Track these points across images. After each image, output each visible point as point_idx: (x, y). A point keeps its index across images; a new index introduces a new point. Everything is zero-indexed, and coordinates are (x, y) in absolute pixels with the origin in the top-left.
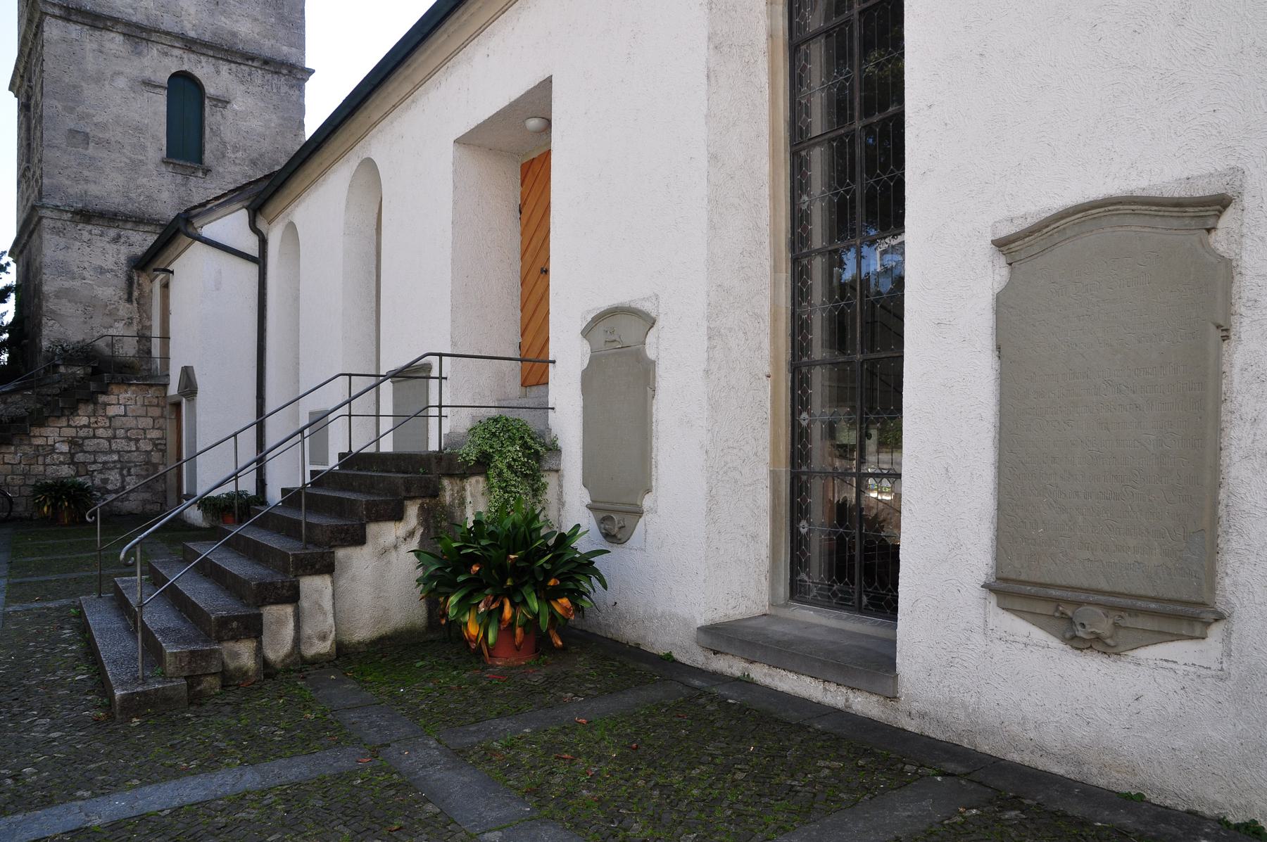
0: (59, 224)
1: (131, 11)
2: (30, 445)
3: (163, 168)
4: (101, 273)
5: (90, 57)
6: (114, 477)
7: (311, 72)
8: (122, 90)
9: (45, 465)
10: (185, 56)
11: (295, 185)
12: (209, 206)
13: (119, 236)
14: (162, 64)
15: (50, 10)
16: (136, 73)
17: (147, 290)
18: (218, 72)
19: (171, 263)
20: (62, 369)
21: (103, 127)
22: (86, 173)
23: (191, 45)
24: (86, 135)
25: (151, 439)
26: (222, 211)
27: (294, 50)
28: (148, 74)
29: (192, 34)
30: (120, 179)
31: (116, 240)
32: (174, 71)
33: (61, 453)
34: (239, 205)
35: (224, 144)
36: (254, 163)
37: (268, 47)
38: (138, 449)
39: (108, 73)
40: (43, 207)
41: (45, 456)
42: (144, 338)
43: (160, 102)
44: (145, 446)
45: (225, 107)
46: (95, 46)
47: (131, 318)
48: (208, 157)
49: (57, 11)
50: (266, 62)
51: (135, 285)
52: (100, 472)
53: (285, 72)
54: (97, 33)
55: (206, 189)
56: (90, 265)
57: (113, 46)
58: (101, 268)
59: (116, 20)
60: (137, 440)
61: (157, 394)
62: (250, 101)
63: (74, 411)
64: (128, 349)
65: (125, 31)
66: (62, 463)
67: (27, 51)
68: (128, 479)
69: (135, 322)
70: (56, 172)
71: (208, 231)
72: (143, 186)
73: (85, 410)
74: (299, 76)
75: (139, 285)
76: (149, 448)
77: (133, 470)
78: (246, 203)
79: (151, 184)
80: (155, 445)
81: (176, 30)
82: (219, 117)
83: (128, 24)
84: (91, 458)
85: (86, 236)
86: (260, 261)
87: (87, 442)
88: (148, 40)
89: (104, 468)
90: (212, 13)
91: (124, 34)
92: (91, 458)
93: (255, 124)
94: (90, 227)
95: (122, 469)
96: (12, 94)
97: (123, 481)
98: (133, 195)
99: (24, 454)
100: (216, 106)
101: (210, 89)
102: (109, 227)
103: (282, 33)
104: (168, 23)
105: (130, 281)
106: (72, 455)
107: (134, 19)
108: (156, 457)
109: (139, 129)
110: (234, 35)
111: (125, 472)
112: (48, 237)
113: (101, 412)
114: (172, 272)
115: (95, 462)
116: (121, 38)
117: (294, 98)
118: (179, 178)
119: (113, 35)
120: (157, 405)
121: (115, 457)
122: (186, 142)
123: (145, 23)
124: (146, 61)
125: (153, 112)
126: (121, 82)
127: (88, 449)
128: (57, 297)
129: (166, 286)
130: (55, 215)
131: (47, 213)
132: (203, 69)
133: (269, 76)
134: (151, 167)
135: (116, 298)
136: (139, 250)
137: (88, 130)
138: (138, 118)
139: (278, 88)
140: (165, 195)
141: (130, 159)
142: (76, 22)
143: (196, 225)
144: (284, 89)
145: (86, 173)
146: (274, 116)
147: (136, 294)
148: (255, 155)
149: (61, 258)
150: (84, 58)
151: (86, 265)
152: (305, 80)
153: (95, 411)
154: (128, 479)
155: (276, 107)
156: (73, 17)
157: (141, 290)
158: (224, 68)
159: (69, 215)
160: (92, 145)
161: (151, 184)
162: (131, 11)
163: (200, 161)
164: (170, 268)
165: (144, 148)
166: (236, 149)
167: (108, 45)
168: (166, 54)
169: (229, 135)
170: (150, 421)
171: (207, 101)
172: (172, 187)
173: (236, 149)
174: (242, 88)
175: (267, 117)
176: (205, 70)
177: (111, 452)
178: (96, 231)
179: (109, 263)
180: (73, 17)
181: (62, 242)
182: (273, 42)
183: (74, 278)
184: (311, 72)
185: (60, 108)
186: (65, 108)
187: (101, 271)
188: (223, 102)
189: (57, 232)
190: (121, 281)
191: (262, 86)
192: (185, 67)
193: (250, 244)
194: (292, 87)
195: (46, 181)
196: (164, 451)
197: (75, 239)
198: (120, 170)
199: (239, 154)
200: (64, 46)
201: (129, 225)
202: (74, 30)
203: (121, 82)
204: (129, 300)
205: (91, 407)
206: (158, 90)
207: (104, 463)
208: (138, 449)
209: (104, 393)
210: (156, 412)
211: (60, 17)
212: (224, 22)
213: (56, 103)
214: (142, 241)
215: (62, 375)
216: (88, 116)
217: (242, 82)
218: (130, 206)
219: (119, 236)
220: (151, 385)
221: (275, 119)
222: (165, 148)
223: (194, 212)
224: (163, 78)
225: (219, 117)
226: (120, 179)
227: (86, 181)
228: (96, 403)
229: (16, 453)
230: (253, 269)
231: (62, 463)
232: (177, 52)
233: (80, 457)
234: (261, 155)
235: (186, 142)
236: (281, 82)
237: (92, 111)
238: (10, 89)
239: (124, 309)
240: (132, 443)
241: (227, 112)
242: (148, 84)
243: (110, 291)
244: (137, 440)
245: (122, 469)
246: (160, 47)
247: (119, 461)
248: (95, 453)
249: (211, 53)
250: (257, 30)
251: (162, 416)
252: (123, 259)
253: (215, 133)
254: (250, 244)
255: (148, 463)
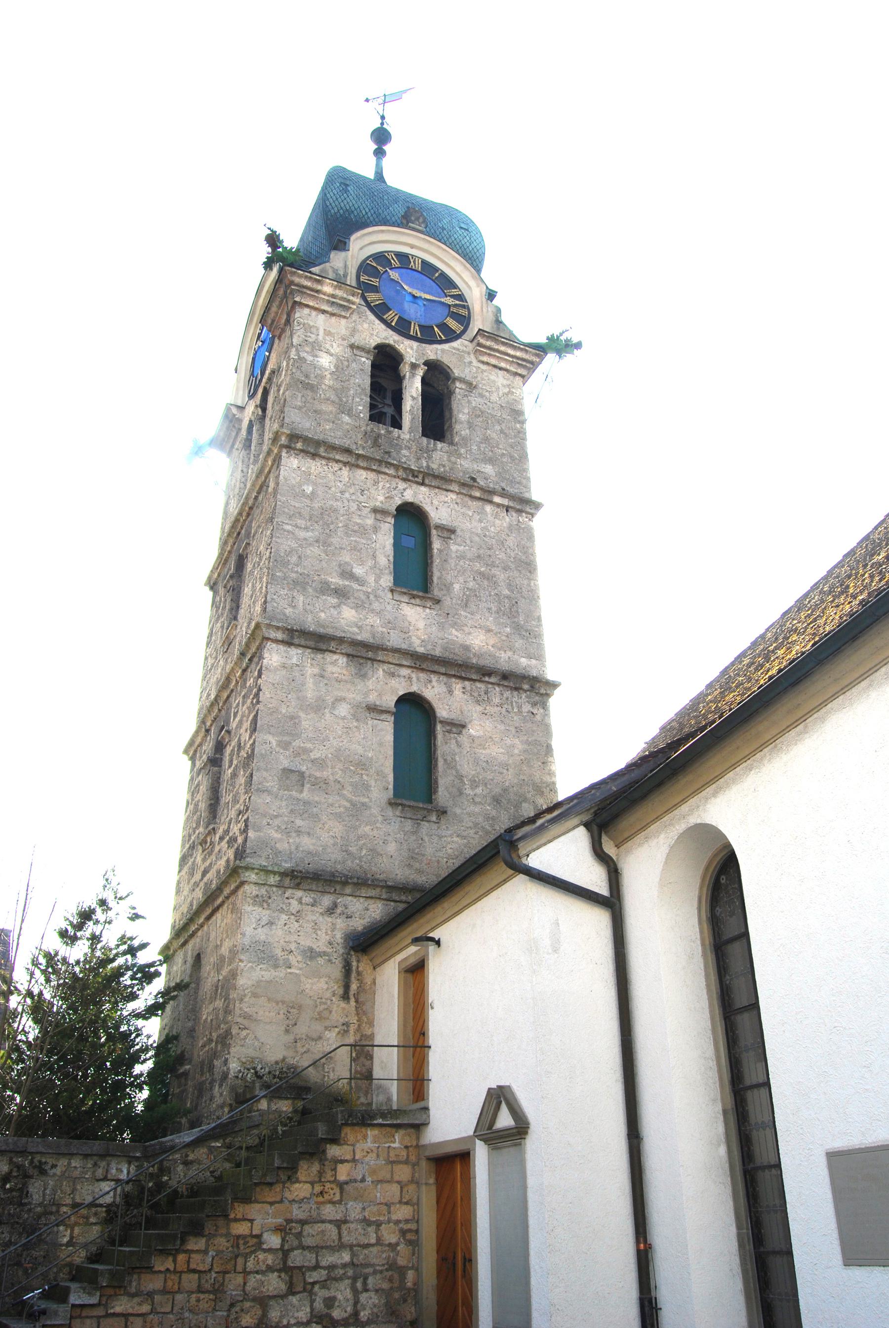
0: (263, 891)
1: (355, 630)
2: (228, 1235)
3: (390, 812)
4: (311, 958)
5: (310, 683)
6: (342, 1292)
7: (554, 685)
8: (344, 718)
9: (246, 1273)
10: (414, 675)
11: (714, 761)
12: (540, 822)
13: (335, 905)
14: (387, 686)
15: (273, 634)
16: (359, 698)
17: (368, 980)
18: (450, 692)
19: (433, 929)
20: (264, 1105)
21: (320, 763)
22: (299, 822)
23: (422, 662)
24: (302, 774)
25: (398, 1222)
26: (555, 829)
27: (534, 662)
28: (372, 698)
29: (421, 650)
30: (338, 829)
31: (331, 911)
32: (401, 693)
33: (270, 1250)
34: (575, 821)
35: (460, 777)
36: (497, 800)
37: (504, 659)
38: (379, 1242)
39: (329, 699)
40: (247, 868)
41: (246, 1256)
42: (363, 1050)
43: (386, 730)
44: (390, 1236)
45: (460, 733)
46: (316, 670)
47: (346, 1024)
48: (442, 795)
49: (280, 635)
50: (505, 676)
51: (354, 975)
52: (324, 1284)
53: (526, 687)
54: (319, 656)
55: (440, 837)
56: (282, 952)
57: (335, 669)
58: (311, 950)
59: (341, 640)
60: (378, 1224)
61: (407, 1141)
62: (488, 724)
63: (290, 1172)
64: (340, 1070)
65: (350, 650)
66: (270, 1269)
67: (225, 695)
68: (363, 1297)
69: (352, 1028)
70: (264, 822)
71: (541, 858)
72: (365, 836)
73: (307, 1170)
74: (542, 691)
75: (359, 973)
76: (393, 1240)
77: (371, 1281)
78: (586, 817)
79: (375, 833)
80: (403, 1232)
81: (404, 646)
82: (453, 745)
83: (355, 643)
84: (309, 1259)
85: (295, 905)
86: (612, 903)
87: (308, 1229)
88: (373, 660)
89: (330, 1278)
90: (442, 626)
91: (348, 655)
92: (309, 1259)
93: (495, 751)
94: (299, 893)
95: (354, 1279)
96: (186, 758)
97: (356, 1302)
98: (353, 849)
99: (219, 1252)
100: (449, 732)
101: (442, 712)
102: (323, 892)
103: (519, 643)
104: (394, 640)
105: (347, 969)
106: (285, 1253)
107: (359, 638)
108: (403, 1256)
109: (362, 765)
110: (467, 648)
111: (359, 1285)
112: (248, 908)
113: (329, 1175)
114: (438, 943)
115: (317, 1267)
116: (345, 659)
117: (538, 718)
118: (409, 825)
119: (335, 657)
120: (406, 1162)
121: (346, 1257)
122: (417, 779)
123: (371, 641)
124: (370, 684)
125: (379, 741)
126: (343, 710)
127: (308, 1241)
128: (255, 995)
129: (416, 971)
130: (262, 878)
131: (252, 877)
132: (434, 690)
133: (507, 694)
134: (375, 811)
135: (328, 994)
136: (358, 925)
137: (304, 768)
138: (360, 751)
139: (519, 707)
140: (392, 848)
141: (350, 801)
142: (299, 646)
143: (522, 852)
144: (526, 708)
145: (299, 822)
146: (517, 741)
147: (354, 987)
148: (498, 790)
149: (263, 938)
150: (303, 685)
151: (293, 946)
152: (548, 695)
153: (321, 1173)
154: (363, 1297)
155: (518, 730)
156: (296, 641)
157: (361, 981)
158: (458, 686)
159: (277, 878)
160: (307, 786)
161: (375, 833)
162: (355, 630)
163: (430, 800)
164: (435, 934)
165: (367, 787)
166: (474, 784)
167: (330, 668)
168: (393, 675)
169: (467, 768)
170: (396, 1188)
171: (439, 727)
172: (400, 836)
173: (474, 784)
174: (479, 708)
175: (508, 742)
176: (436, 690)
177: (342, 1246)
178: (308, 898)
179: (321, 945)
180: (296, 641)
181: (265, 915)
182: (510, 654)
183: (276, 967)
184: (554, 685)
185: (274, 744)
186: (279, 743)
187: (311, 954)
188: (457, 726)
189: (261, 901)
190: (336, 971)
191: (501, 706)
192: (414, 688)
193: (593, 877)
194: (534, 704)
195: (251, 834)
196: (414, 1244)
197: (282, 911)
198: (338, 816)
199: (479, 791)
200: (284, 672)
201: (348, 890)
202: (295, 655)
203: (343, 710)
204: (345, 997)
205: (316, 1167)
206: (383, 717)
207: (331, 1268)
208: (379, 1242)
209: (335, 1141)
210: (403, 1173)
211: (283, 642)
212: (455, 635)
213: (270, 738)
214: (367, 911)
215: (262, 1113)
216: (307, 751)
217: (478, 702)
218: (349, 863)
219: (335, 905)
220: (398, 1126)
221: (518, 745)
222: (391, 787)
223: (520, 833)
224: (390, 701)
225: (453, 745)
226: (338, 829)
227: (299, 832)
228: (322, 1160)
229: (205, 1252)
230: (597, 921)
231: (270, 1269)
232: (405, 672)
233: (297, 1258)
234: (505, 790)
235: (417, 779)
236: (522, 700)
237: (309, 745)
238: (186, 752)
239: (341, 1011)
240: (371, 1229)
241: (463, 739)
242: (374, 709)
243: (322, 984)
244: (378, 1224)
245: (354, 1279)
246: (386, 667)
247: (352, 1264)
248: (316, 1249)
249: (443, 670)
250: (491, 642)
251: (412, 1181)
252: (339, 936)
253: (451, 765)
254: (593, 877)
255: (392, 1266)
